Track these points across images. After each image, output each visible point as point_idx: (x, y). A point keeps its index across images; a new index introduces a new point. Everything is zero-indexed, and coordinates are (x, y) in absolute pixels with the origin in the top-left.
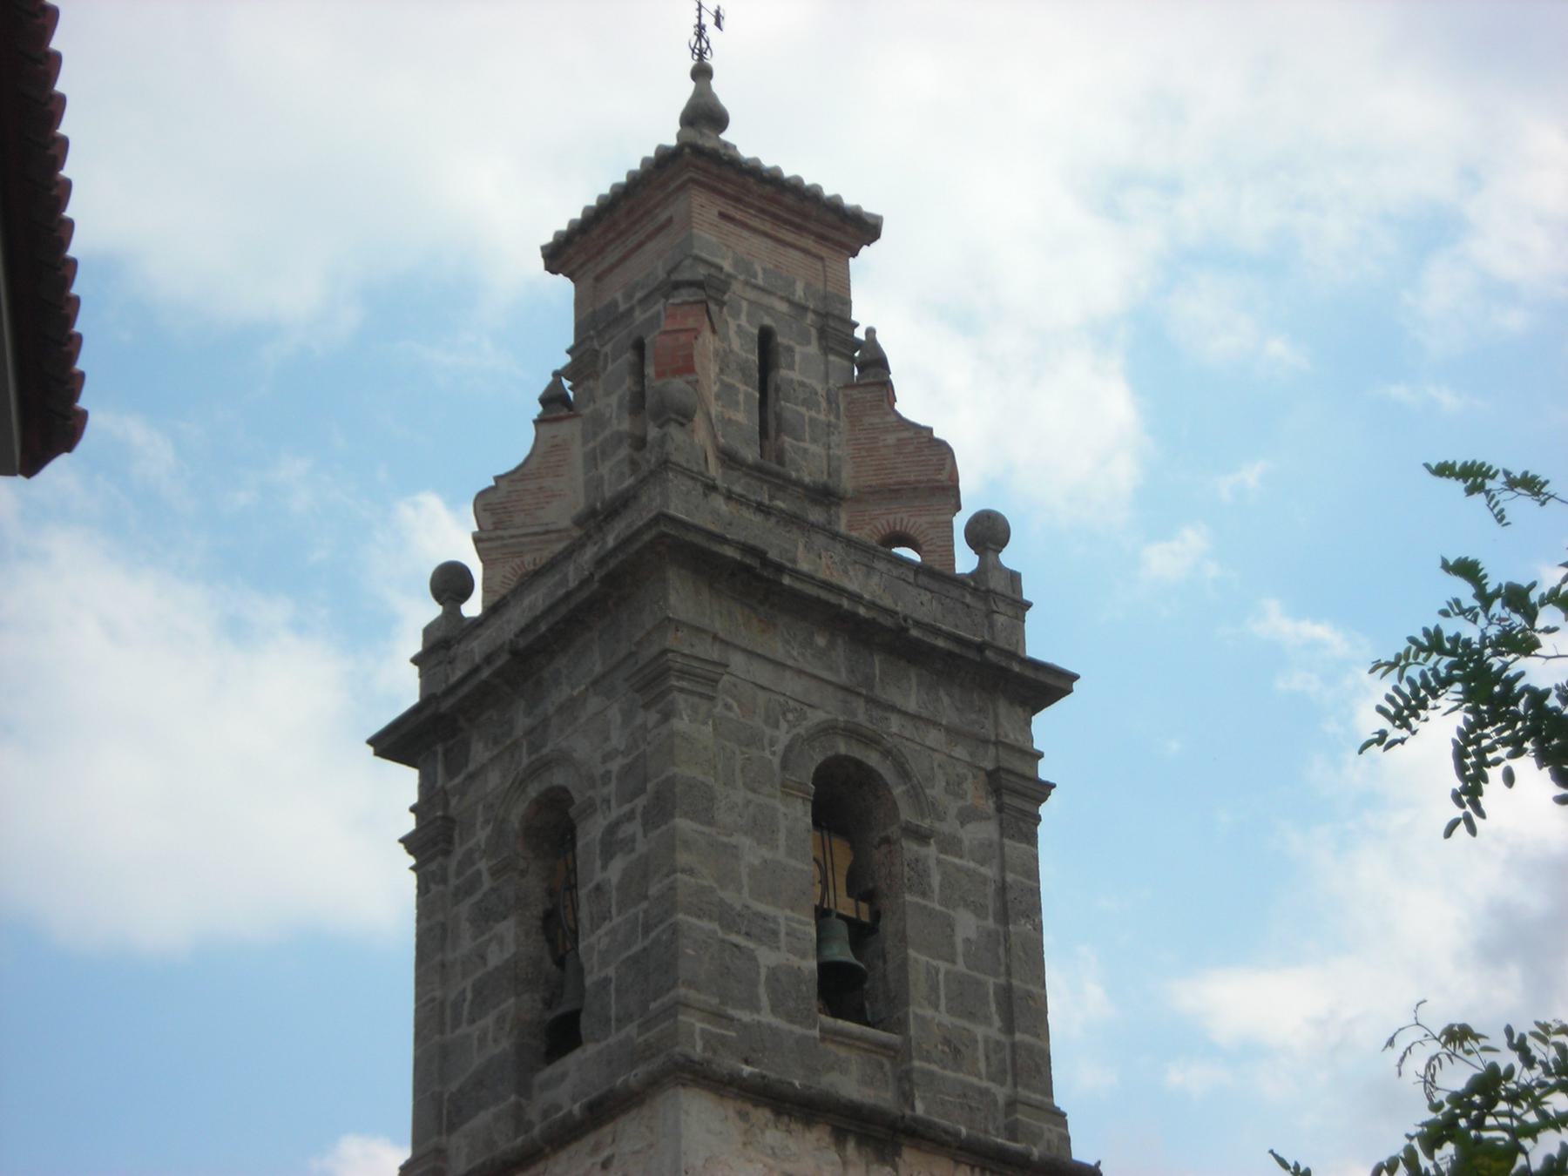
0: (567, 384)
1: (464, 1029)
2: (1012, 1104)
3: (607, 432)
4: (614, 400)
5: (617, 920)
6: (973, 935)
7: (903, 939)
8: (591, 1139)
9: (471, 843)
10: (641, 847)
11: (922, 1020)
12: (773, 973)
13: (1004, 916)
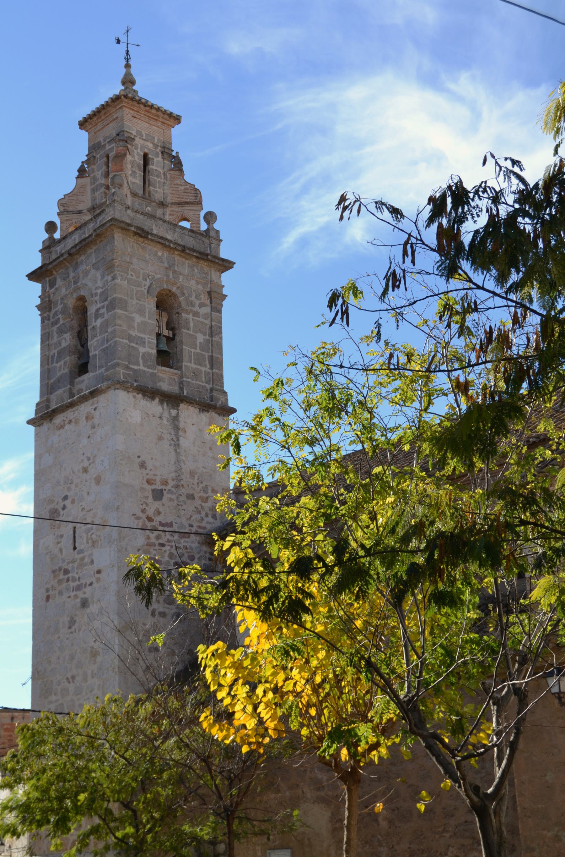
0: (86, 166)
1: (54, 364)
2: (212, 390)
3: (98, 183)
4: (100, 172)
5: (99, 338)
6: (202, 341)
7: (181, 342)
8: (91, 401)
9: (57, 309)
10: (106, 317)
11: (186, 366)
12: (144, 355)
13: (211, 335)
